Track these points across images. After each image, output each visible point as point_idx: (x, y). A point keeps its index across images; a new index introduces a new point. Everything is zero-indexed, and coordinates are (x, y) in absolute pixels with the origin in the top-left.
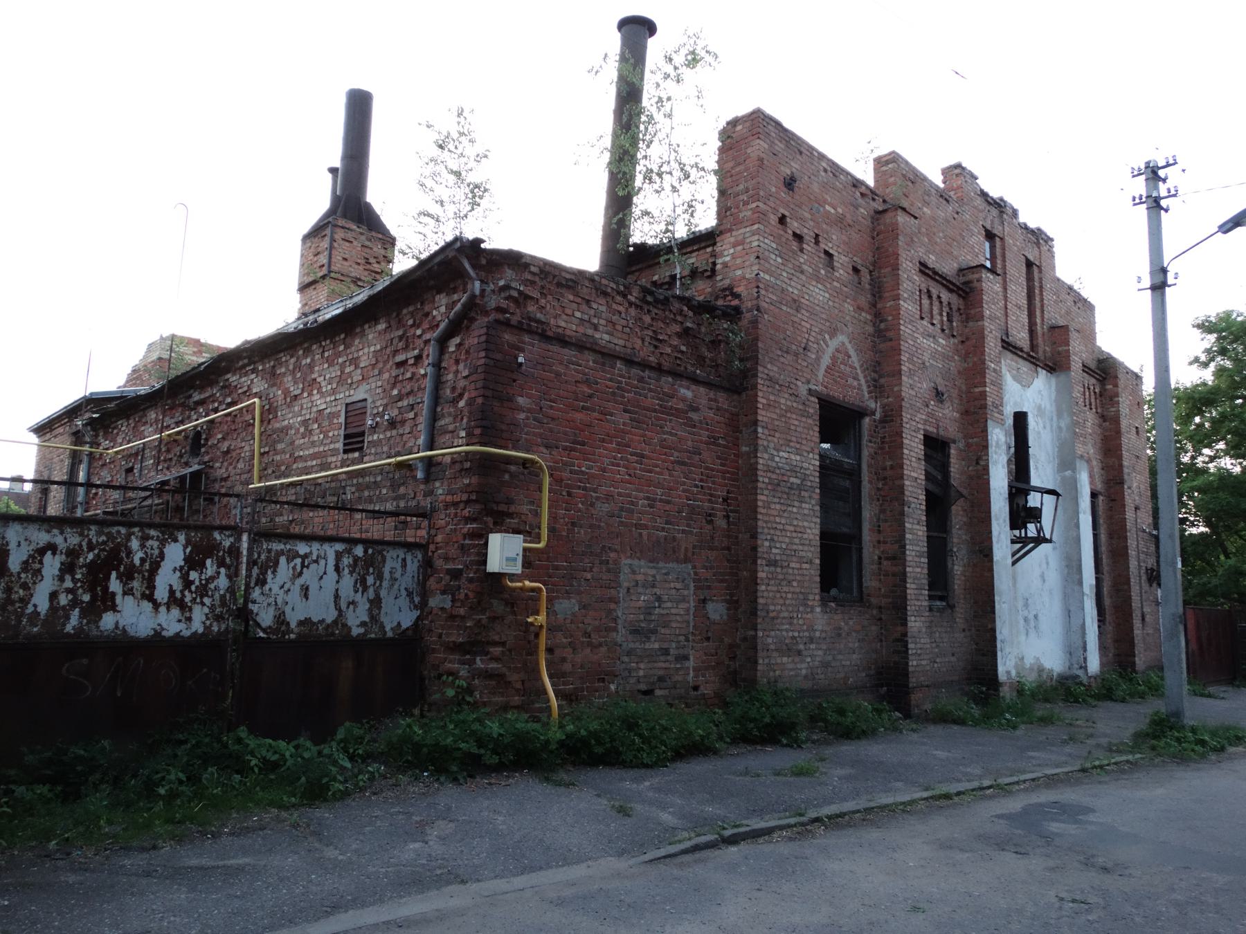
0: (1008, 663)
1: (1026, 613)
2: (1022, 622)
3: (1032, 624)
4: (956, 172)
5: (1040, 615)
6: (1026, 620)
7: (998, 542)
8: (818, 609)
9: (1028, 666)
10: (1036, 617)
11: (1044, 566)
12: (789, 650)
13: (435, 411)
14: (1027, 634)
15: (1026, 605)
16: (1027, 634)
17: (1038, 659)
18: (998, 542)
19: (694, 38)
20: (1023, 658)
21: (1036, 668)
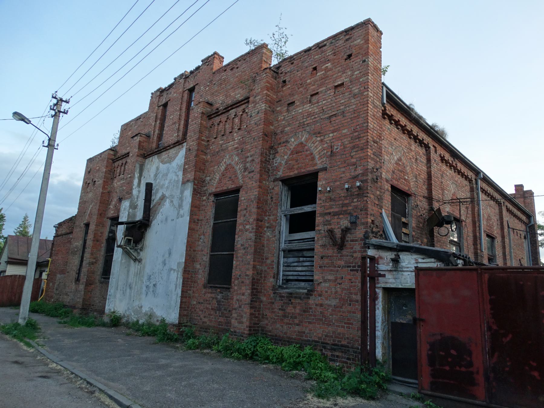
0: (110, 305)
1: (148, 283)
2: (144, 288)
3: (151, 290)
4: (202, 61)
5: (158, 284)
6: (147, 287)
7: (116, 252)
8: (74, 284)
9: (144, 311)
10: (154, 285)
11: (167, 255)
12: (67, 294)
13: (479, 222)
14: (146, 295)
15: (149, 279)
16: (146, 295)
17: (152, 309)
18: (116, 252)
19: (256, 74)
20: (141, 307)
21: (149, 314)
